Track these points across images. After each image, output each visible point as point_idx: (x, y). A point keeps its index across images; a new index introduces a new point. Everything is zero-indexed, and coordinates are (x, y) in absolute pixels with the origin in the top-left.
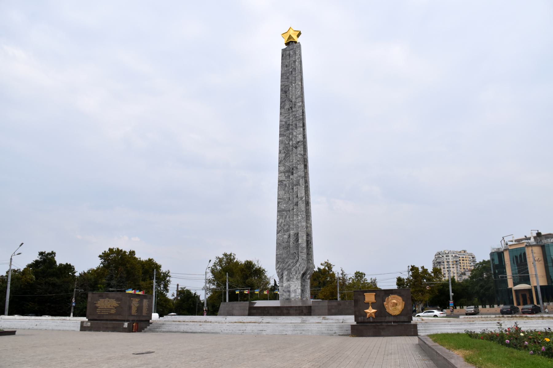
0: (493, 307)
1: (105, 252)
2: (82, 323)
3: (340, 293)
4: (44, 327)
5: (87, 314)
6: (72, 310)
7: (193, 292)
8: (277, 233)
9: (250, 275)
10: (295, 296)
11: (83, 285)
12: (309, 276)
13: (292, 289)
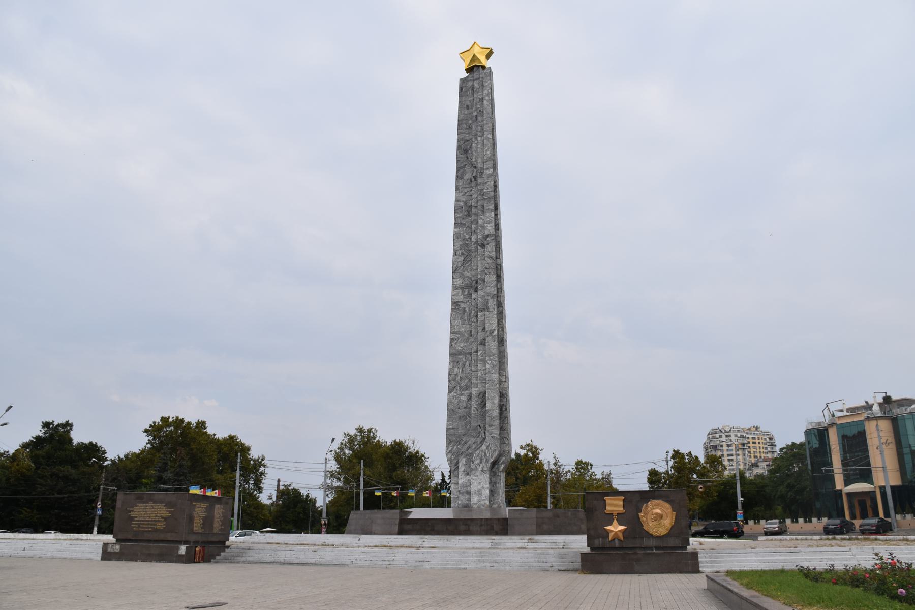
0: (811, 521)
1: (154, 423)
2: (105, 545)
3: (553, 497)
4: (37, 553)
5: (115, 529)
6: (97, 522)
7: (304, 492)
8: (449, 393)
9: (400, 464)
10: (479, 501)
11: (115, 479)
12: (503, 466)
13: (474, 488)
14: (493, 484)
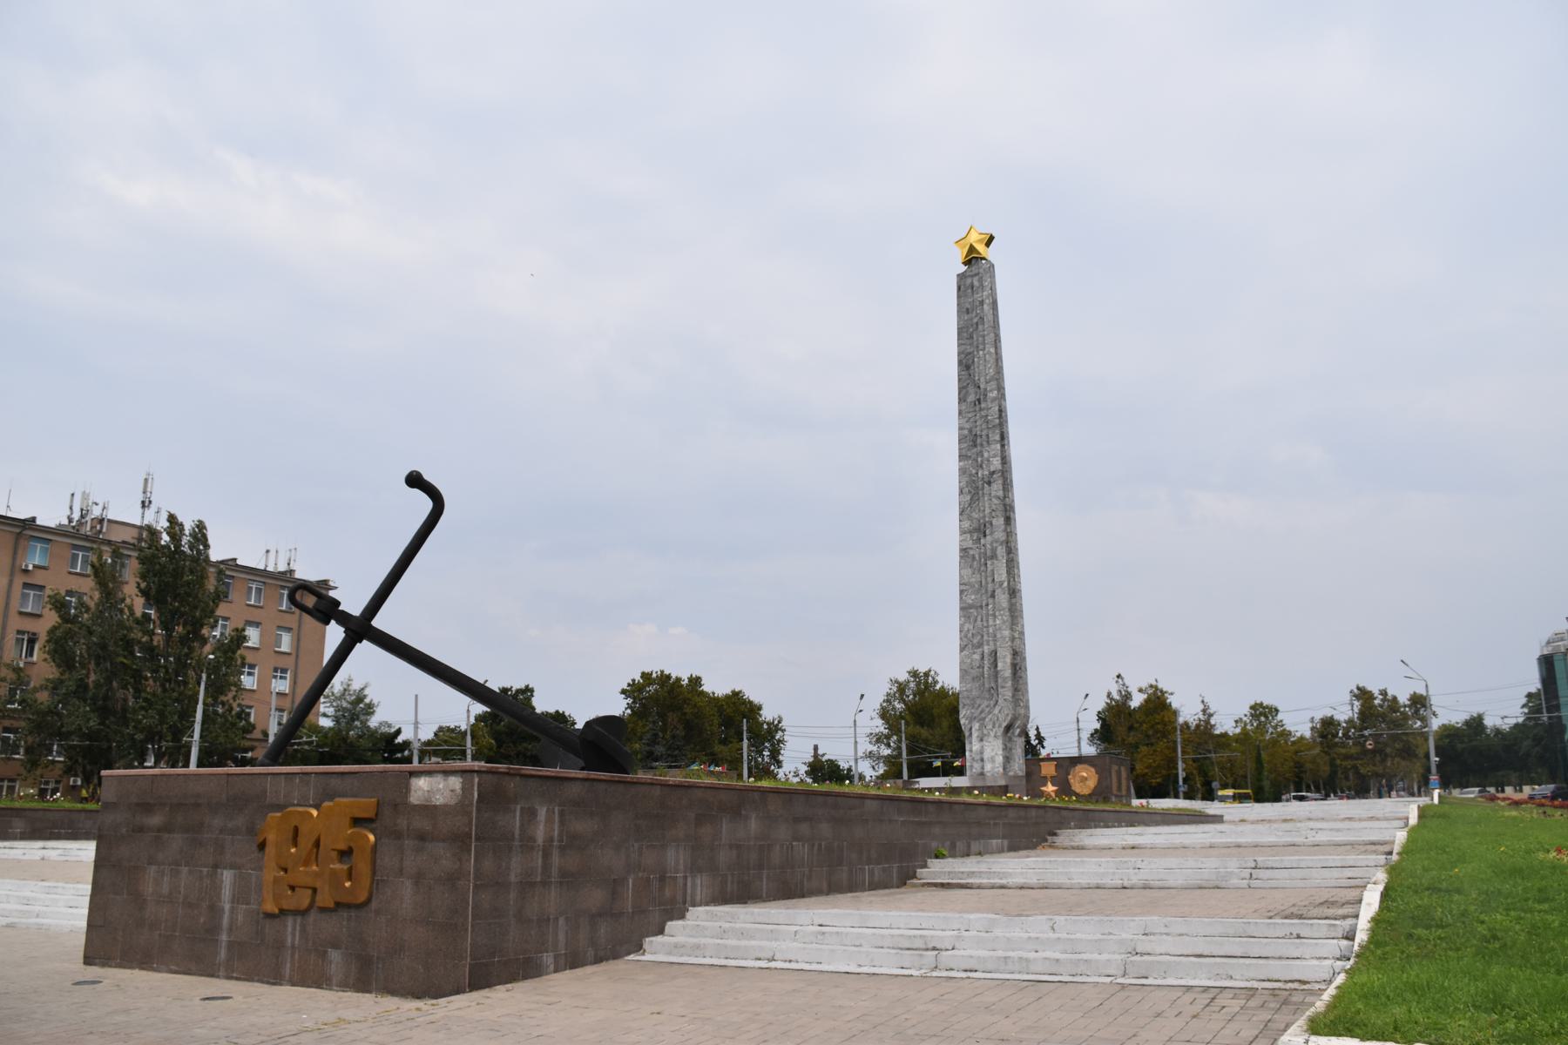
13: (986, 756)
14: (1007, 750)
